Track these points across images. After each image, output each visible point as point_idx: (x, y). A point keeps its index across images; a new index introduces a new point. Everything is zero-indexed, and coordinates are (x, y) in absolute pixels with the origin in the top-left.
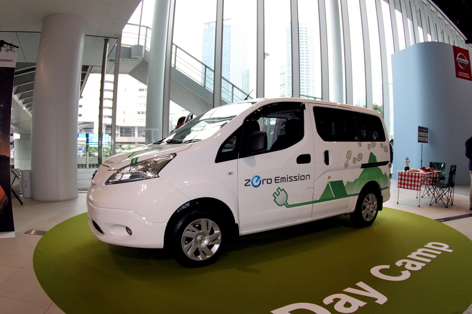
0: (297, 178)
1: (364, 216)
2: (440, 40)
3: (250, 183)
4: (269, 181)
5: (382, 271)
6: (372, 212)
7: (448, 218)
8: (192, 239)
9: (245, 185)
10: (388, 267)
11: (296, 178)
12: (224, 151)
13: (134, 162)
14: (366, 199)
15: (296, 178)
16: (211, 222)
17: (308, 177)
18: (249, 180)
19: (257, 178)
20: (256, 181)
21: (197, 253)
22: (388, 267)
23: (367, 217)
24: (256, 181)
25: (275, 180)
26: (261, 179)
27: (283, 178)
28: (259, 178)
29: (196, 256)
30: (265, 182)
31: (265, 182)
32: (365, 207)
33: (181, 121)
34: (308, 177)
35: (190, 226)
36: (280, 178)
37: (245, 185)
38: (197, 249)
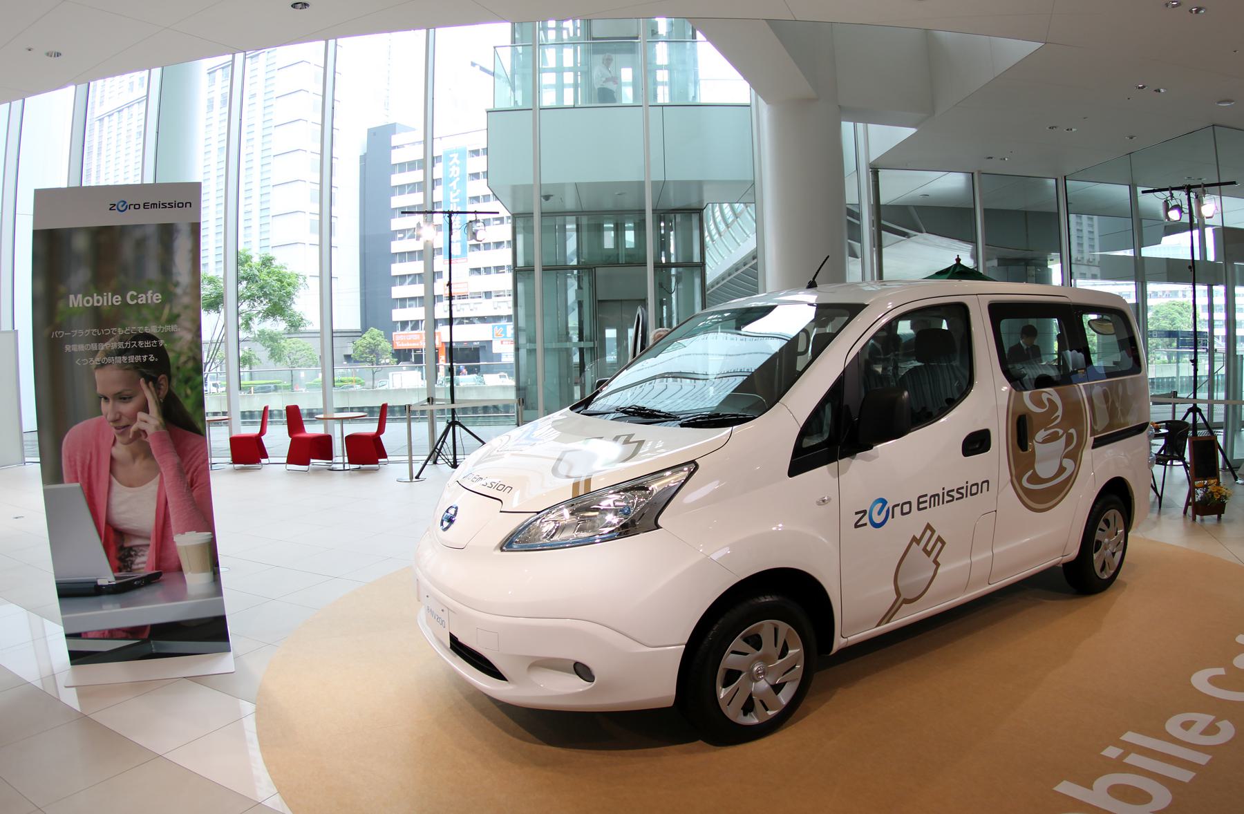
0: (963, 491)
1: (1097, 566)
2: (860, 126)
3: (866, 520)
4: (905, 508)
5: (1214, 681)
6: (1114, 554)
7: (217, 565)
8: (740, 673)
9: (856, 526)
10: (1221, 671)
11: (960, 493)
12: (808, 443)
13: (581, 492)
14: (1102, 525)
15: (960, 493)
16: (784, 627)
17: (985, 485)
18: (865, 512)
19: (880, 505)
20: (879, 513)
21: (748, 707)
22: (1221, 671)
23: (1103, 569)
24: (879, 513)
25: (919, 503)
26: (890, 505)
27: (934, 496)
28: (884, 502)
29: (745, 714)
30: (898, 510)
31: (898, 510)
32: (1099, 543)
33: (1105, 394)
34: (985, 485)
35: (738, 643)
36: (927, 498)
37: (856, 526)
38: (750, 697)
